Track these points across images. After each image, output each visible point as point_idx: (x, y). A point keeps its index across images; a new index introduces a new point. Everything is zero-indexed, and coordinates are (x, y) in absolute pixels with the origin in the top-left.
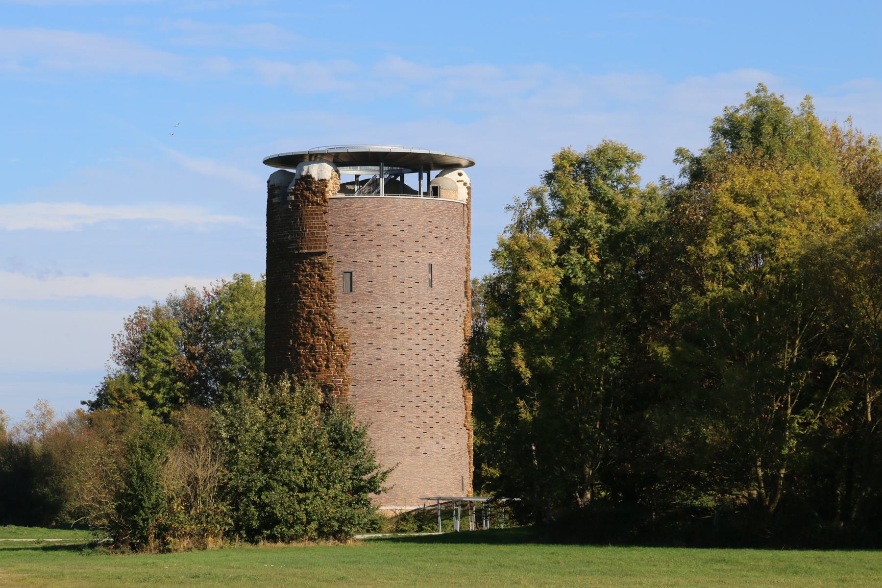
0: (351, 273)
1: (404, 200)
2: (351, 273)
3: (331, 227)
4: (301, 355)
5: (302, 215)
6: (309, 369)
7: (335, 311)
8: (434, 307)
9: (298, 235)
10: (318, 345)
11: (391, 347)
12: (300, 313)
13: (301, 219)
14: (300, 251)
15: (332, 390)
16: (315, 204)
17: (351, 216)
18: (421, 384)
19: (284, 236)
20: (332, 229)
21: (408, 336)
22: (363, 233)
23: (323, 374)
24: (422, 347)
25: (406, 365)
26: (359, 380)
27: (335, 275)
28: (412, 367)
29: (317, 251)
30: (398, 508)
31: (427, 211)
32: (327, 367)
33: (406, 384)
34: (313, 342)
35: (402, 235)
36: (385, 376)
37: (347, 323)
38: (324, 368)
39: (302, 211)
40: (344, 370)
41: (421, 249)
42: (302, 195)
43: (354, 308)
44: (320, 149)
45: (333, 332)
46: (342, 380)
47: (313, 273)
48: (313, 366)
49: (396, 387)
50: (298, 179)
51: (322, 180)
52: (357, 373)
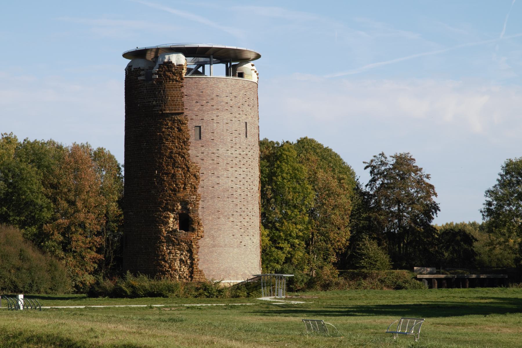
0: (200, 127)
1: (232, 80)
2: (200, 127)
3: (186, 97)
4: (165, 181)
5: (165, 88)
6: (171, 190)
7: (189, 152)
8: (248, 150)
9: (162, 101)
10: (178, 174)
11: (225, 176)
12: (164, 153)
13: (164, 91)
14: (164, 112)
15: (188, 204)
16: (175, 81)
17: (200, 90)
18: (243, 200)
19: (150, 102)
20: (187, 98)
21: (234, 169)
22: (207, 101)
23: (181, 193)
24: (242, 176)
25: (234, 188)
26: (206, 198)
27: (189, 128)
28: (238, 189)
29: (176, 112)
30: (232, 281)
31: (244, 88)
32: (184, 188)
33: (234, 200)
34: (174, 172)
35: (231, 103)
36: (222, 195)
37: (198, 160)
38: (182, 189)
39: (165, 86)
40: (196, 191)
41: (241, 113)
42: (165, 75)
43: (202, 150)
44: (167, 45)
45: (189, 166)
46: (195, 197)
47: (173, 127)
48: (174, 188)
49: (229, 202)
50: (161, 64)
51: (180, 65)
52: (205, 193)
